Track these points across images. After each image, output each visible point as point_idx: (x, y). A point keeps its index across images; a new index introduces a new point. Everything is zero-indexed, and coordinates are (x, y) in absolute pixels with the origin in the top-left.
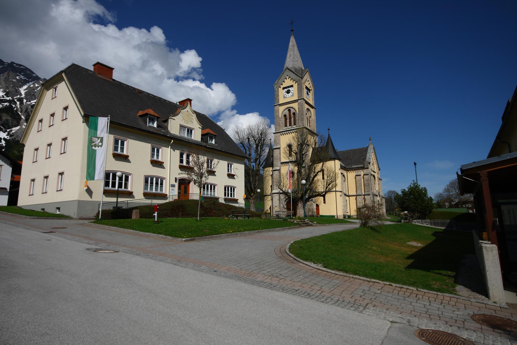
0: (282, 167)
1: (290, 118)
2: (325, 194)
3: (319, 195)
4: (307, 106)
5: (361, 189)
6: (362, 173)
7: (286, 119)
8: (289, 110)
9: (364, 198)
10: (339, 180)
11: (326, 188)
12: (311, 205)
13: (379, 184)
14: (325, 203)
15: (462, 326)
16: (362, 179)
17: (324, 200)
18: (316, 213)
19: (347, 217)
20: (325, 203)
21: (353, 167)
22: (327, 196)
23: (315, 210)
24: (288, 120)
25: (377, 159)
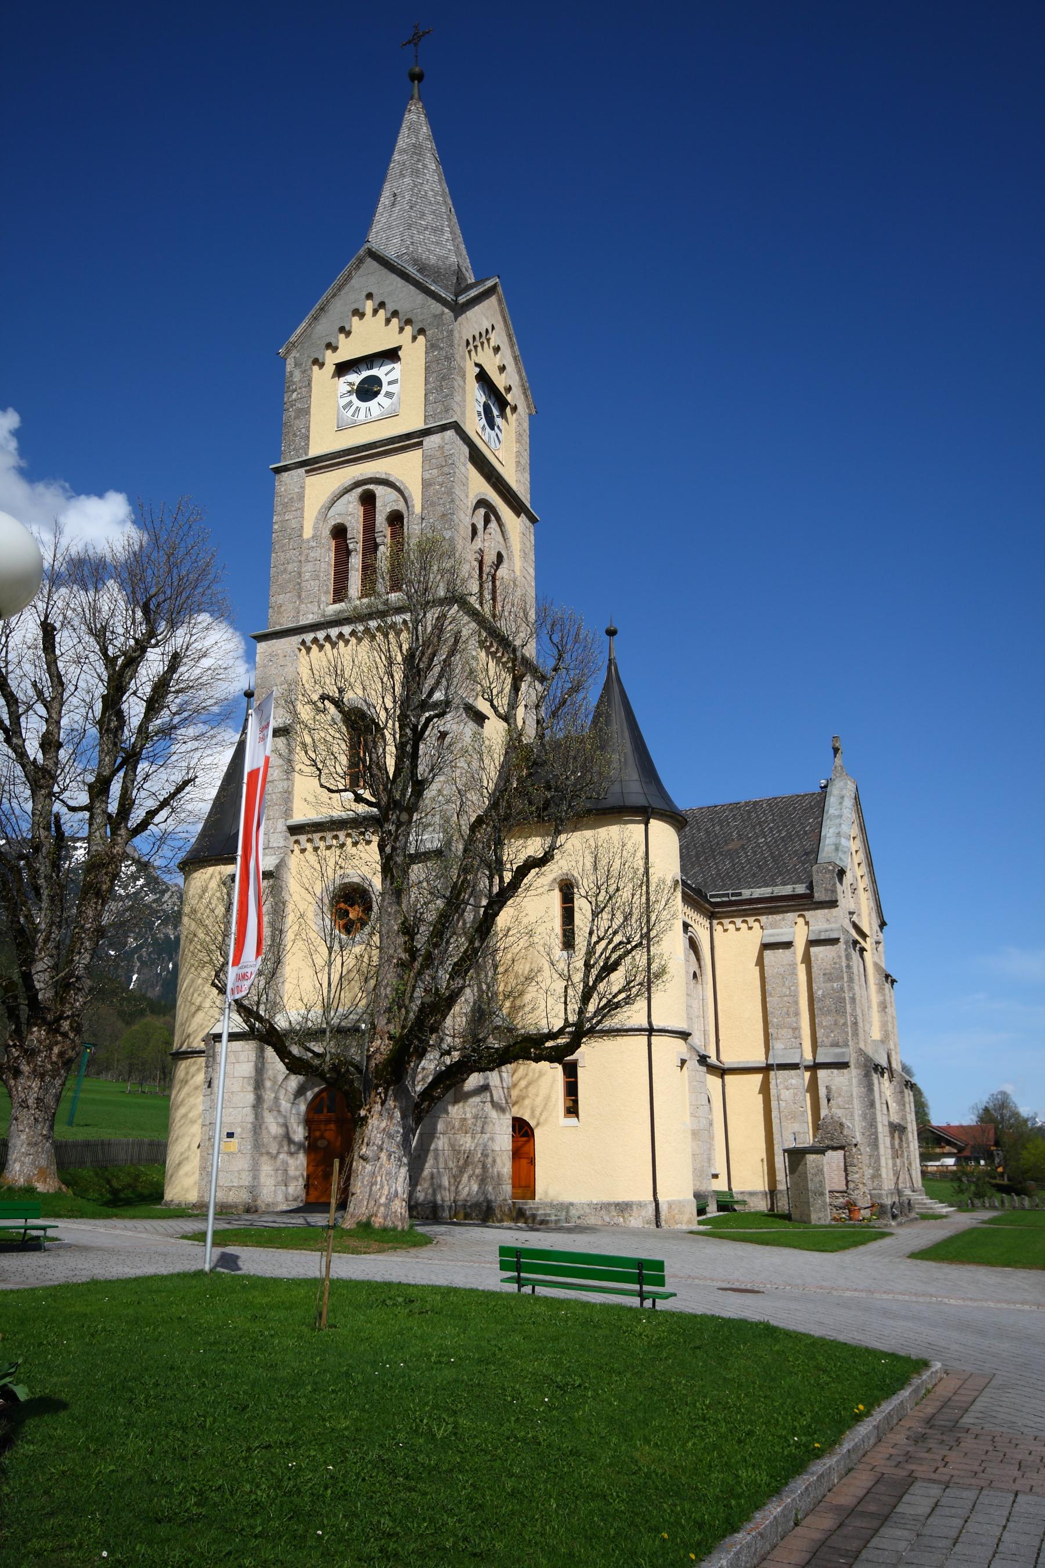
0: (295, 861)
1: (371, 547)
2: (574, 1045)
3: (531, 1047)
4: (479, 486)
5: (796, 1029)
6: (795, 928)
7: (343, 553)
8: (368, 500)
9: (813, 1087)
10: (671, 947)
11: (586, 998)
12: (475, 1129)
13: (883, 1007)
14: (572, 1110)
15: (991, 1448)
16: (802, 969)
17: (572, 1089)
18: (507, 1188)
19: (712, 1211)
20: (572, 1110)
21: (746, 894)
22: (590, 1055)
23: (504, 1166)
24: (356, 561)
25: (870, 865)
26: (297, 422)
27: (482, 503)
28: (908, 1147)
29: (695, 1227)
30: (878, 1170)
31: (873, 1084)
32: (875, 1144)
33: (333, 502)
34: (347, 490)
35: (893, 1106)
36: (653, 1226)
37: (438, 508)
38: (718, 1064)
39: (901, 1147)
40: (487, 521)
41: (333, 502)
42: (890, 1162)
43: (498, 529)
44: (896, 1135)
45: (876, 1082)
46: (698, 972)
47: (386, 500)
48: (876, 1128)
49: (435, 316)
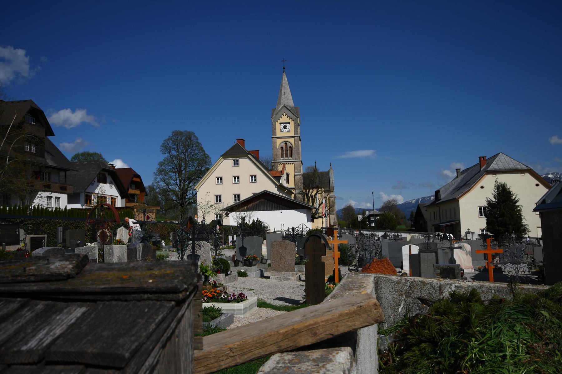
8: (286, 144)
14: (334, 271)
47: (289, 145)
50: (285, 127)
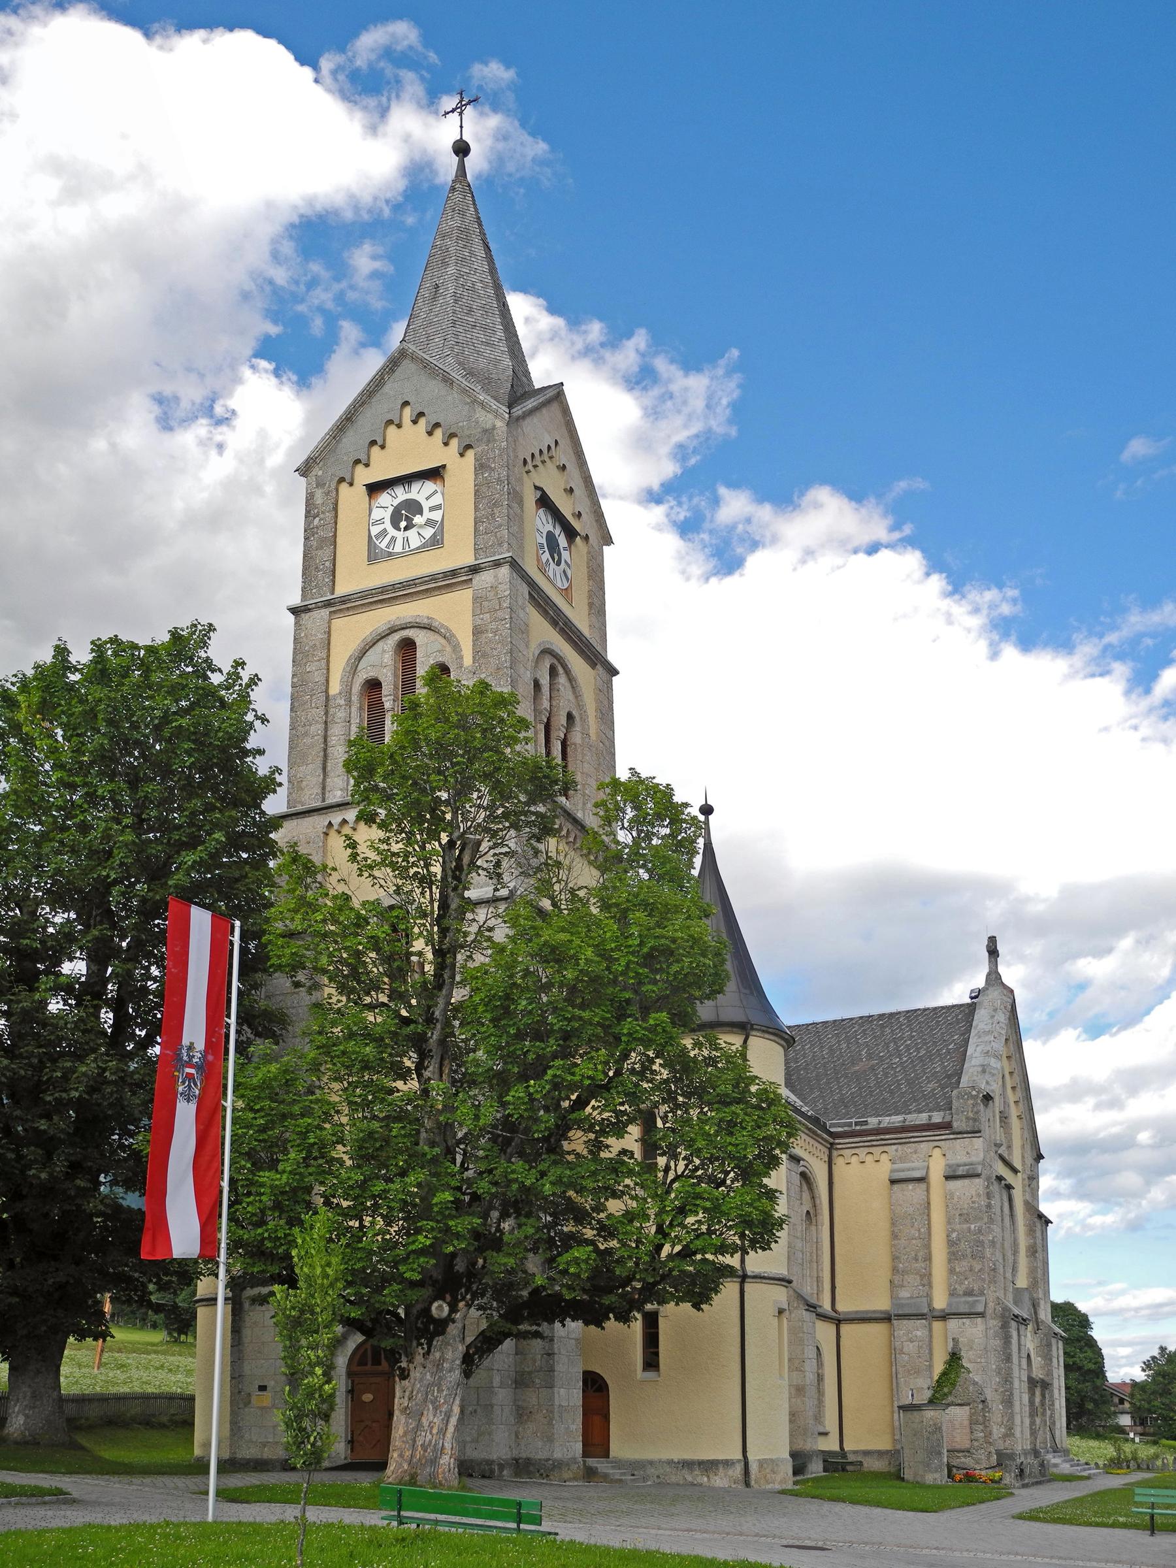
6: (936, 1159)
8: (407, 648)
14: (651, 1362)
19: (816, 1468)
20: (651, 1362)
26: (320, 553)
27: (547, 652)
28: (1053, 1405)
29: (790, 1486)
30: (1011, 1429)
31: (1011, 1337)
32: (1008, 1402)
33: (363, 652)
34: (383, 637)
35: (1037, 1361)
36: (741, 1486)
37: (491, 660)
38: (834, 1314)
39: (1043, 1404)
40: (553, 672)
41: (363, 652)
42: (1027, 1421)
43: (568, 685)
44: (1038, 1392)
45: (1014, 1334)
46: (812, 1212)
48: (1011, 1383)
49: (485, 431)
50: (405, 514)
